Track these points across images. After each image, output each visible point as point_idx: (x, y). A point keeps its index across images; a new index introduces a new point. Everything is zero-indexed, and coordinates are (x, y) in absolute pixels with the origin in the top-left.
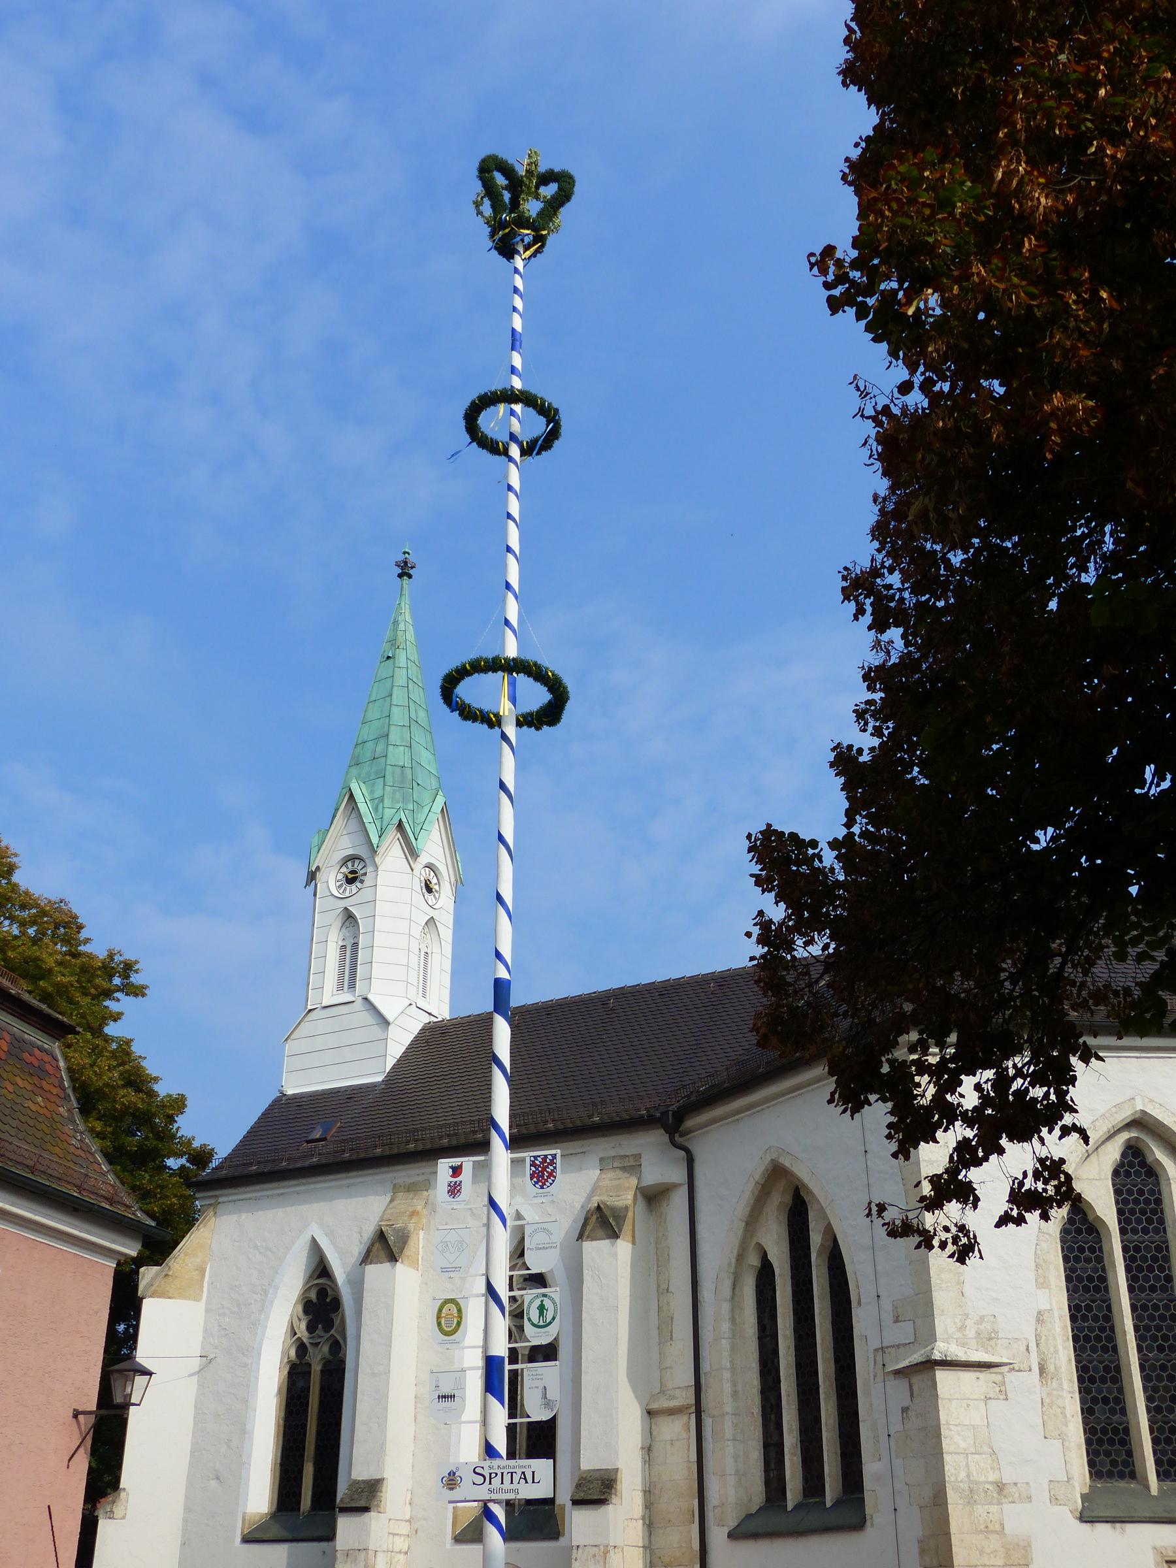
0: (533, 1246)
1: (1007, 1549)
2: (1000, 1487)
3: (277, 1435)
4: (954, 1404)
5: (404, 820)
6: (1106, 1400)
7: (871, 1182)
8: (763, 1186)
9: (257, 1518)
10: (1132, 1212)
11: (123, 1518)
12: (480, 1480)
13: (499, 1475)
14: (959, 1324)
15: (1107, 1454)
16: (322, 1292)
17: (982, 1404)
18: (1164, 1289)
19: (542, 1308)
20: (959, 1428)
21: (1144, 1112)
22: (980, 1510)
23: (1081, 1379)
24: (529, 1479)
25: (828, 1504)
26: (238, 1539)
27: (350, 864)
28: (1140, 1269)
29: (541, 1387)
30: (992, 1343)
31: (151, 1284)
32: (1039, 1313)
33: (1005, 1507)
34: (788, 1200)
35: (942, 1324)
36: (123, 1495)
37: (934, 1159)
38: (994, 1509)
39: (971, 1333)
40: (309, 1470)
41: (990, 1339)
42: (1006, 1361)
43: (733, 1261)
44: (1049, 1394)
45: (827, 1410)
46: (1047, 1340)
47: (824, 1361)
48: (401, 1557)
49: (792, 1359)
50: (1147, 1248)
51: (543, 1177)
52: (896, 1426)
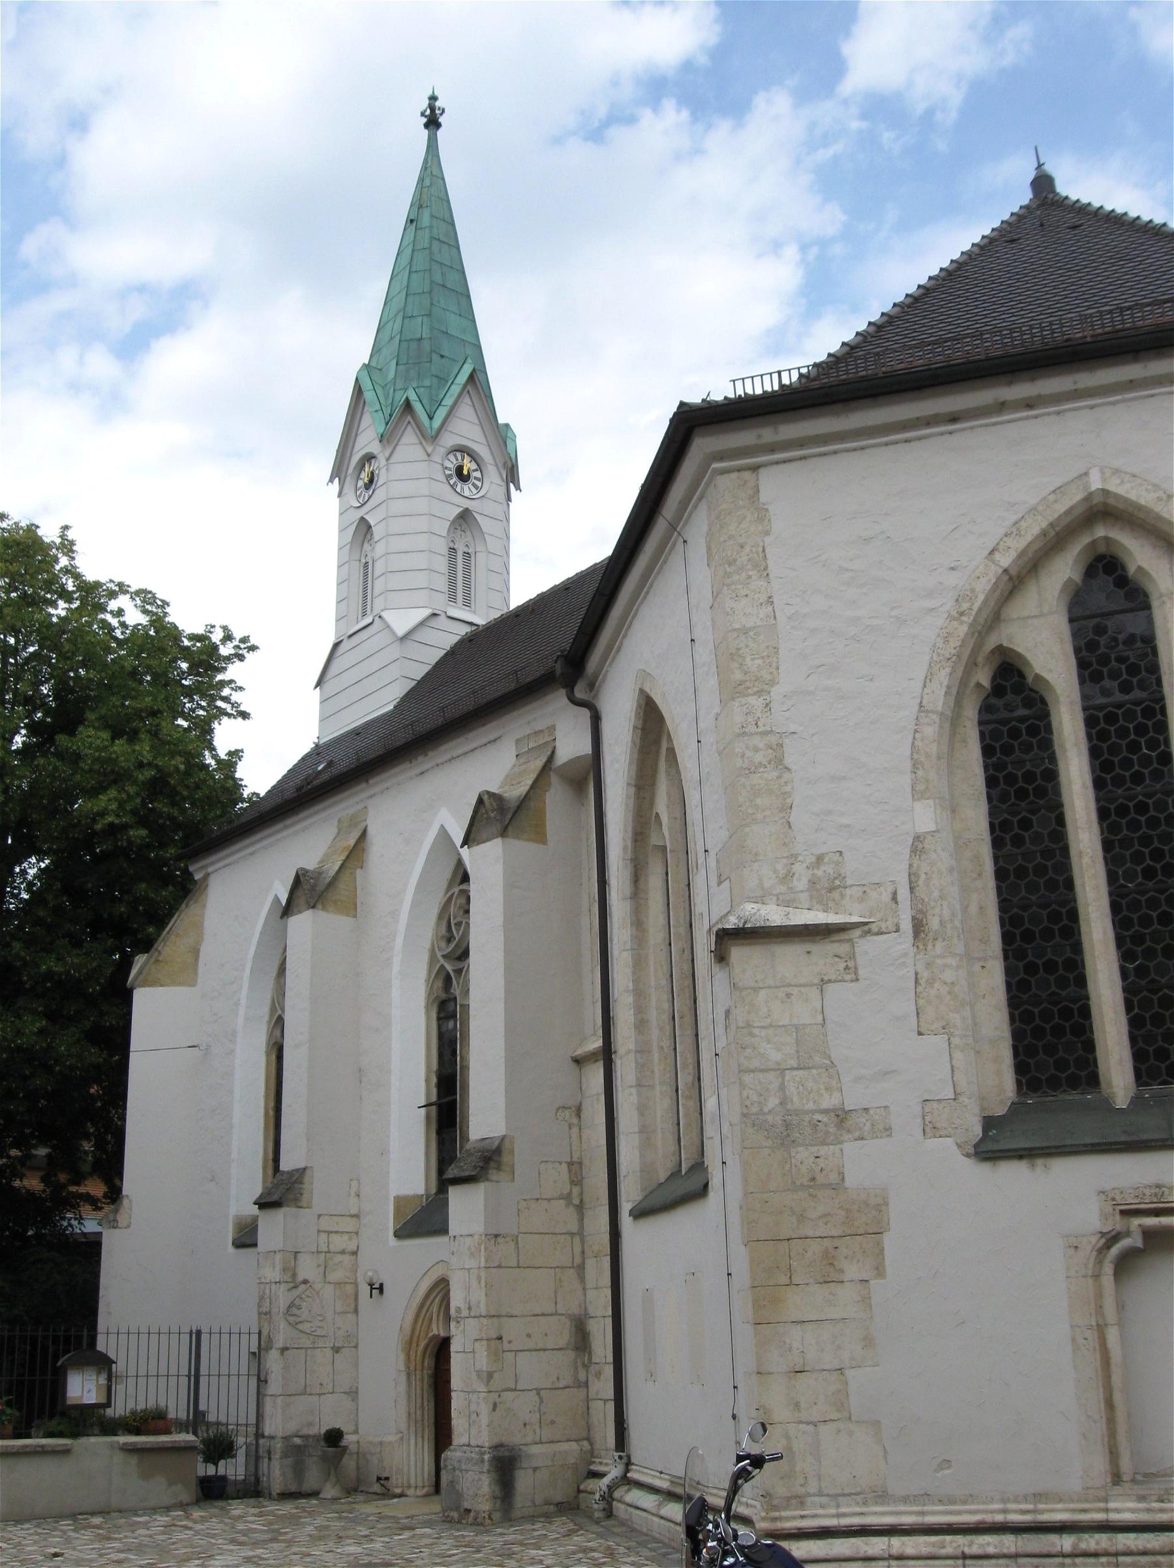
1: (848, 1211)
2: (841, 1116)
4: (763, 994)
5: (413, 397)
6: (1050, 967)
8: (643, 729)
11: (128, 1226)
14: (782, 873)
17: (814, 993)
18: (1157, 775)
20: (770, 1031)
21: (1105, 492)
22: (803, 1154)
23: (1007, 938)
31: (140, 972)
32: (918, 838)
33: (847, 1147)
36: (125, 1202)
39: (801, 883)
41: (831, 890)
42: (855, 919)
43: (629, 843)
44: (929, 965)
46: (928, 879)
48: (346, 1259)
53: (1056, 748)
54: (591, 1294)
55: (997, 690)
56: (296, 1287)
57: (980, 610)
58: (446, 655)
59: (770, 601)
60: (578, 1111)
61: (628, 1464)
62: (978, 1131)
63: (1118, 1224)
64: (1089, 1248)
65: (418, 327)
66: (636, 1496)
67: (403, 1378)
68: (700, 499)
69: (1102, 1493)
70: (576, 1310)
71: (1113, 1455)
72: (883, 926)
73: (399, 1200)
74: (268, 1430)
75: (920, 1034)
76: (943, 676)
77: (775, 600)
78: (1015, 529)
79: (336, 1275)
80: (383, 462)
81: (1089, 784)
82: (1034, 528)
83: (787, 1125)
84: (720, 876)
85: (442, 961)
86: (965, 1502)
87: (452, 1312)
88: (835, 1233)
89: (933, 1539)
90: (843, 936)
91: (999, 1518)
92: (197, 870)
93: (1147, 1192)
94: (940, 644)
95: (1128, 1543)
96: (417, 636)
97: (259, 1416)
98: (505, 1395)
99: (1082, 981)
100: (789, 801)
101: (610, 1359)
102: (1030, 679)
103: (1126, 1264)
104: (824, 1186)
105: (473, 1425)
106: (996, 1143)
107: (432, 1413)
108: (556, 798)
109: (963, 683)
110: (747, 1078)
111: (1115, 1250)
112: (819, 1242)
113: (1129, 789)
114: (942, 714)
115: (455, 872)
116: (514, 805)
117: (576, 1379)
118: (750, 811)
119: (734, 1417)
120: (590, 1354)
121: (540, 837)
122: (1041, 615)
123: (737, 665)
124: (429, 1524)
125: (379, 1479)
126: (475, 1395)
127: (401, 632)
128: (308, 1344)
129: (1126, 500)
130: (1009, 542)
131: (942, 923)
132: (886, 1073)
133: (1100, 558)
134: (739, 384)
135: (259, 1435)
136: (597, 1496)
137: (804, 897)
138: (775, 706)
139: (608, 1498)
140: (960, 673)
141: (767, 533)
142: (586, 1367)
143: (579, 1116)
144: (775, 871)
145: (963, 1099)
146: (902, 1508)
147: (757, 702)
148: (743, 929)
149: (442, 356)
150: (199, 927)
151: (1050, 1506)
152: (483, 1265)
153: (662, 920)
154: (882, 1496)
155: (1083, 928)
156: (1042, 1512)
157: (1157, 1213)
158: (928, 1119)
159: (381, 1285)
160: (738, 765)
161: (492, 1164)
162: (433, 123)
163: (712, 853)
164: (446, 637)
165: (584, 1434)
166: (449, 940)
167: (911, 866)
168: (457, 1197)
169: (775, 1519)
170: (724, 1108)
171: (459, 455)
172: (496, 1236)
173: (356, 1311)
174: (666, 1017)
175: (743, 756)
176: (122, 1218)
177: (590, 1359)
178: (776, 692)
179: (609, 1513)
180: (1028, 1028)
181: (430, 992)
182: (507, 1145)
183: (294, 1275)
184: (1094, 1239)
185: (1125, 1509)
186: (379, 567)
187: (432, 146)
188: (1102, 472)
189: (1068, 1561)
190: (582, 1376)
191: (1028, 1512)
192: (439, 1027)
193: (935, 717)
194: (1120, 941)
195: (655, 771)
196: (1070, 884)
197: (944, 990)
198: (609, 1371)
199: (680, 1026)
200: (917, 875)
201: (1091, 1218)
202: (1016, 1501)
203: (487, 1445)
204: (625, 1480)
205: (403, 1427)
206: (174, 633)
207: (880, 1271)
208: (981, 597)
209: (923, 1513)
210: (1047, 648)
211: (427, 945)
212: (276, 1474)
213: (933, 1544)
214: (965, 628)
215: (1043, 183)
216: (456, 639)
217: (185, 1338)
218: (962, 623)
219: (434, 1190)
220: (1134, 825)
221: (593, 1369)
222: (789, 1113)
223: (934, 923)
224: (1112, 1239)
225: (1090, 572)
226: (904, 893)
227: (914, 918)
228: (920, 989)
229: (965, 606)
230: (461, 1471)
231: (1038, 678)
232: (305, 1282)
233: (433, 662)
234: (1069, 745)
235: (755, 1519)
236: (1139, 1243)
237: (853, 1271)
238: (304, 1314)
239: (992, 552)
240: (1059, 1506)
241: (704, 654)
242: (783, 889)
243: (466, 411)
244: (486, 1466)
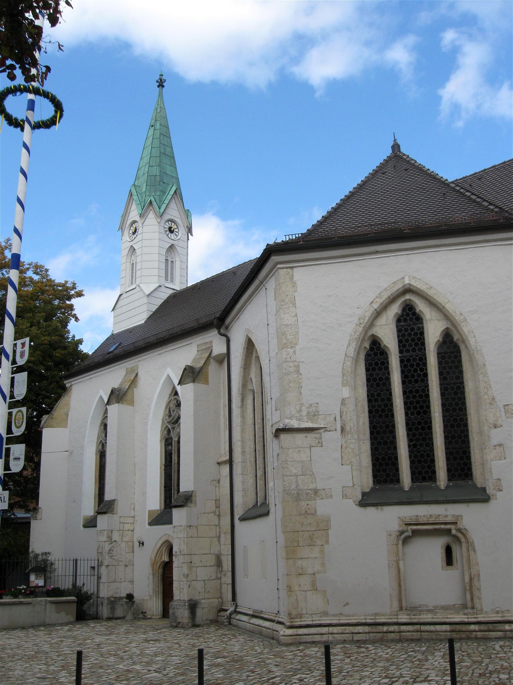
2: (316, 491)
4: (291, 450)
5: (153, 200)
6: (385, 443)
8: (247, 349)
10: (407, 341)
11: (41, 519)
15: (385, 471)
17: (308, 450)
22: (303, 503)
23: (372, 433)
26: (147, 523)
30: (316, 417)
31: (45, 422)
32: (343, 400)
33: (317, 501)
36: (40, 510)
39: (304, 413)
41: (314, 416)
43: (241, 388)
48: (130, 533)
50: (414, 360)
53: (390, 370)
54: (223, 547)
55: (371, 349)
56: (112, 543)
57: (367, 322)
58: (164, 302)
59: (296, 315)
60: (219, 481)
61: (236, 606)
62: (360, 497)
63: (405, 528)
64: (394, 535)
65: (156, 171)
66: (240, 617)
67: (151, 577)
68: (273, 275)
69: (396, 613)
70: (217, 552)
71: (400, 601)
72: (331, 428)
73: (150, 511)
74: (101, 595)
75: (342, 465)
76: (354, 345)
77: (298, 315)
78: (380, 296)
79: (126, 539)
80: (141, 225)
81: (401, 383)
82: (385, 296)
83: (298, 494)
84: (276, 408)
85: (167, 424)
86: (353, 616)
87: (174, 553)
88: (313, 529)
89: (343, 628)
90: (317, 431)
91: (364, 621)
92: (67, 383)
93: (414, 518)
94: (353, 334)
95: (404, 628)
96: (153, 295)
97: (98, 590)
98: (193, 582)
99: (395, 448)
100: (301, 385)
101: (230, 569)
102: (382, 346)
103: (405, 541)
104: (310, 514)
105: (181, 592)
106: (366, 501)
107: (162, 588)
108: (212, 368)
109: (360, 347)
110: (285, 478)
111: (403, 536)
112: (307, 534)
113: (413, 385)
114: (353, 358)
115: (172, 392)
116: (198, 370)
117: (217, 577)
118: (288, 388)
119: (278, 589)
120: (222, 568)
121: (206, 382)
122: (387, 325)
123: (284, 337)
124: (166, 628)
125: (142, 612)
127: (147, 293)
128: (116, 564)
129: (416, 287)
130: (377, 300)
131: (350, 428)
132: (331, 477)
133: (407, 305)
134: (287, 237)
135: (98, 597)
136: (226, 617)
137: (305, 418)
138: (297, 352)
139: (229, 618)
140: (359, 344)
141: (296, 291)
142: (220, 572)
143: (219, 483)
144: (296, 409)
145: (356, 487)
146: (333, 618)
147: (291, 351)
148: (285, 428)
149: (164, 183)
150: (68, 404)
151: (379, 617)
152: (185, 536)
153: (251, 416)
154: (325, 614)
155: (396, 430)
156: (377, 619)
157: (416, 524)
158: (344, 493)
159: (143, 542)
160: (284, 372)
161: (189, 501)
163: (274, 400)
164: (164, 295)
165: (220, 596)
166: (170, 416)
167: (341, 409)
168: (176, 513)
169: (292, 622)
170: (276, 486)
171: (170, 222)
172: (190, 526)
173: (133, 552)
174: (253, 450)
175: (286, 369)
176: (39, 517)
177: (222, 569)
178: (298, 348)
179: (230, 623)
180: (377, 463)
182: (194, 494)
183: (111, 539)
184: (396, 533)
185: (403, 618)
186: (139, 266)
187: (161, 95)
188: (409, 278)
189: (385, 634)
190: (219, 576)
191: (373, 619)
192: (165, 448)
193: (351, 359)
194: (408, 435)
195: (251, 360)
196: (393, 415)
197: (351, 450)
198: (230, 574)
199: (259, 454)
200: (343, 412)
201: (395, 526)
202: (369, 616)
203: (187, 599)
204: (235, 612)
205: (151, 593)
206: (51, 283)
207: (327, 542)
208: (367, 318)
209: (339, 620)
210: (388, 335)
211: (161, 418)
212: (105, 611)
213: (343, 629)
214: (361, 329)
215: (396, 147)
216: (168, 295)
217: (72, 562)
218: (360, 327)
219: (163, 508)
220: (414, 397)
221: (223, 573)
222: (299, 490)
223: (348, 428)
224: (402, 533)
225: (404, 310)
226: (338, 418)
227: (341, 426)
228: (343, 450)
229: (362, 321)
231: (385, 346)
232: (115, 541)
233: (159, 305)
234: (394, 370)
235: (285, 622)
236: (410, 534)
237: (319, 542)
238: (115, 553)
239: (371, 303)
240: (383, 617)
241: (272, 330)
242: (298, 415)
243: (173, 205)
244: (186, 607)
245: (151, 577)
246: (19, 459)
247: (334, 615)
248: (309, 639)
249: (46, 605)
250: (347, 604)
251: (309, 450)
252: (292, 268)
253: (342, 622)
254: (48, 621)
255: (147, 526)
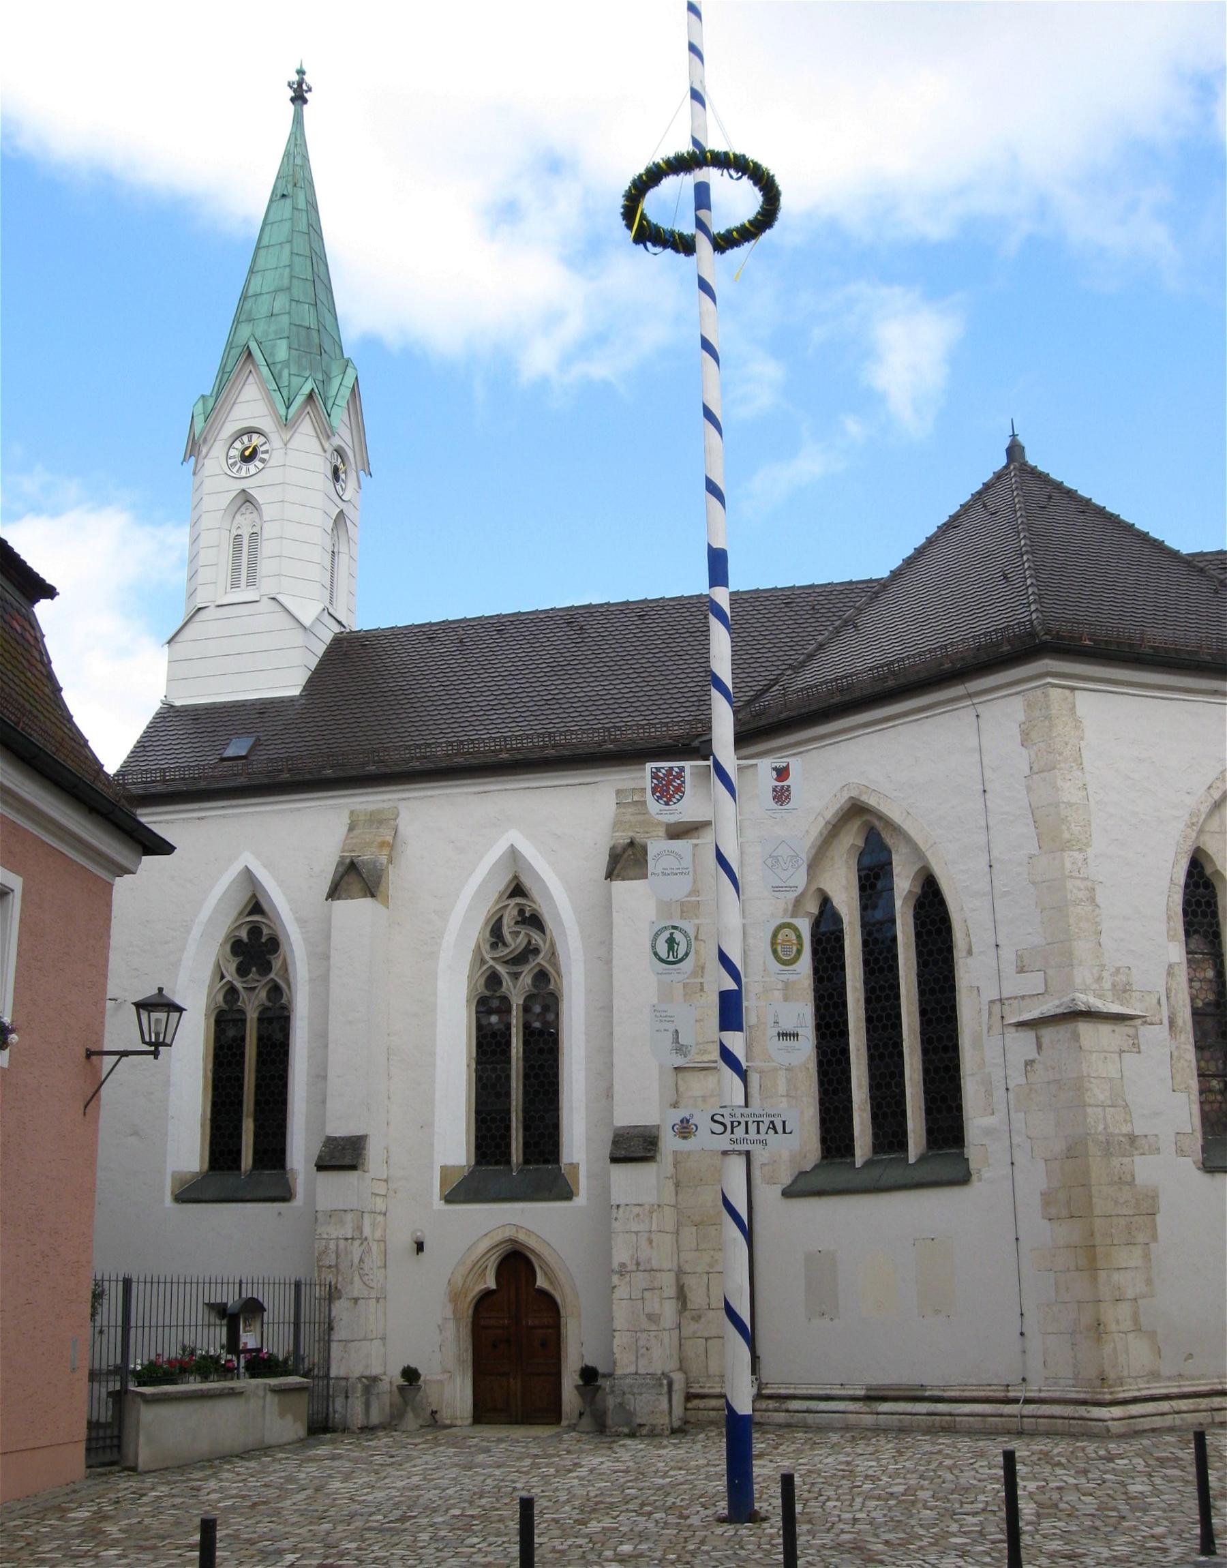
0: (659, 870)
2: (1132, 1139)
3: (205, 1089)
4: (1094, 1055)
7: (990, 824)
8: (834, 826)
9: (188, 1177)
12: (720, 1128)
13: (743, 1124)
14: (1096, 975)
16: (255, 931)
17: (1116, 1057)
19: (671, 942)
22: (1115, 1161)
24: (779, 1128)
25: (912, 1160)
27: (245, 438)
28: (930, 953)
29: (672, 1029)
30: (1126, 995)
32: (1170, 966)
33: (1137, 1159)
34: (860, 843)
35: (1083, 975)
37: (1073, 801)
38: (1126, 1160)
39: (1107, 985)
40: (248, 1127)
41: (1125, 991)
43: (790, 908)
45: (912, 1065)
46: (1176, 994)
47: (909, 1014)
48: (380, 1218)
49: (862, 1013)
51: (667, 791)
52: (1017, 1078)
73: (444, 1169)
79: (378, 1234)
85: (491, 963)
86: (1199, 1379)
97: (328, 1360)
119: (1022, 1334)
126: (645, 1335)
141: (1082, 739)
162: (299, 96)
173: (385, 1267)
181: (472, 988)
186: (266, 549)
187: (298, 121)
192: (478, 1019)
197: (1186, 1064)
207: (1155, 1238)
215: (1014, 451)
229: (1195, 820)
230: (634, 1394)
237: (1141, 1238)
245: (451, 1326)
246: (795, 1035)
247: (1169, 1378)
248: (1158, 1422)
249: (264, 1397)
250: (1190, 1356)
251: (1117, 1058)
252: (1073, 689)
253: (1186, 1390)
254: (270, 1439)
255: (438, 1204)
